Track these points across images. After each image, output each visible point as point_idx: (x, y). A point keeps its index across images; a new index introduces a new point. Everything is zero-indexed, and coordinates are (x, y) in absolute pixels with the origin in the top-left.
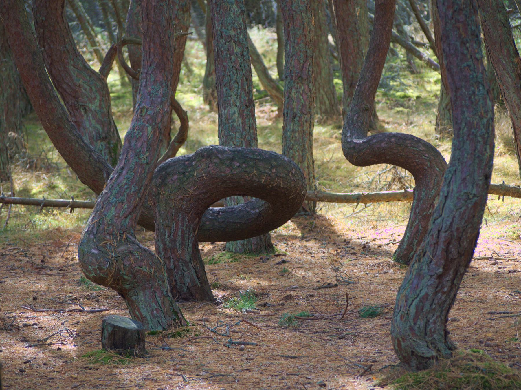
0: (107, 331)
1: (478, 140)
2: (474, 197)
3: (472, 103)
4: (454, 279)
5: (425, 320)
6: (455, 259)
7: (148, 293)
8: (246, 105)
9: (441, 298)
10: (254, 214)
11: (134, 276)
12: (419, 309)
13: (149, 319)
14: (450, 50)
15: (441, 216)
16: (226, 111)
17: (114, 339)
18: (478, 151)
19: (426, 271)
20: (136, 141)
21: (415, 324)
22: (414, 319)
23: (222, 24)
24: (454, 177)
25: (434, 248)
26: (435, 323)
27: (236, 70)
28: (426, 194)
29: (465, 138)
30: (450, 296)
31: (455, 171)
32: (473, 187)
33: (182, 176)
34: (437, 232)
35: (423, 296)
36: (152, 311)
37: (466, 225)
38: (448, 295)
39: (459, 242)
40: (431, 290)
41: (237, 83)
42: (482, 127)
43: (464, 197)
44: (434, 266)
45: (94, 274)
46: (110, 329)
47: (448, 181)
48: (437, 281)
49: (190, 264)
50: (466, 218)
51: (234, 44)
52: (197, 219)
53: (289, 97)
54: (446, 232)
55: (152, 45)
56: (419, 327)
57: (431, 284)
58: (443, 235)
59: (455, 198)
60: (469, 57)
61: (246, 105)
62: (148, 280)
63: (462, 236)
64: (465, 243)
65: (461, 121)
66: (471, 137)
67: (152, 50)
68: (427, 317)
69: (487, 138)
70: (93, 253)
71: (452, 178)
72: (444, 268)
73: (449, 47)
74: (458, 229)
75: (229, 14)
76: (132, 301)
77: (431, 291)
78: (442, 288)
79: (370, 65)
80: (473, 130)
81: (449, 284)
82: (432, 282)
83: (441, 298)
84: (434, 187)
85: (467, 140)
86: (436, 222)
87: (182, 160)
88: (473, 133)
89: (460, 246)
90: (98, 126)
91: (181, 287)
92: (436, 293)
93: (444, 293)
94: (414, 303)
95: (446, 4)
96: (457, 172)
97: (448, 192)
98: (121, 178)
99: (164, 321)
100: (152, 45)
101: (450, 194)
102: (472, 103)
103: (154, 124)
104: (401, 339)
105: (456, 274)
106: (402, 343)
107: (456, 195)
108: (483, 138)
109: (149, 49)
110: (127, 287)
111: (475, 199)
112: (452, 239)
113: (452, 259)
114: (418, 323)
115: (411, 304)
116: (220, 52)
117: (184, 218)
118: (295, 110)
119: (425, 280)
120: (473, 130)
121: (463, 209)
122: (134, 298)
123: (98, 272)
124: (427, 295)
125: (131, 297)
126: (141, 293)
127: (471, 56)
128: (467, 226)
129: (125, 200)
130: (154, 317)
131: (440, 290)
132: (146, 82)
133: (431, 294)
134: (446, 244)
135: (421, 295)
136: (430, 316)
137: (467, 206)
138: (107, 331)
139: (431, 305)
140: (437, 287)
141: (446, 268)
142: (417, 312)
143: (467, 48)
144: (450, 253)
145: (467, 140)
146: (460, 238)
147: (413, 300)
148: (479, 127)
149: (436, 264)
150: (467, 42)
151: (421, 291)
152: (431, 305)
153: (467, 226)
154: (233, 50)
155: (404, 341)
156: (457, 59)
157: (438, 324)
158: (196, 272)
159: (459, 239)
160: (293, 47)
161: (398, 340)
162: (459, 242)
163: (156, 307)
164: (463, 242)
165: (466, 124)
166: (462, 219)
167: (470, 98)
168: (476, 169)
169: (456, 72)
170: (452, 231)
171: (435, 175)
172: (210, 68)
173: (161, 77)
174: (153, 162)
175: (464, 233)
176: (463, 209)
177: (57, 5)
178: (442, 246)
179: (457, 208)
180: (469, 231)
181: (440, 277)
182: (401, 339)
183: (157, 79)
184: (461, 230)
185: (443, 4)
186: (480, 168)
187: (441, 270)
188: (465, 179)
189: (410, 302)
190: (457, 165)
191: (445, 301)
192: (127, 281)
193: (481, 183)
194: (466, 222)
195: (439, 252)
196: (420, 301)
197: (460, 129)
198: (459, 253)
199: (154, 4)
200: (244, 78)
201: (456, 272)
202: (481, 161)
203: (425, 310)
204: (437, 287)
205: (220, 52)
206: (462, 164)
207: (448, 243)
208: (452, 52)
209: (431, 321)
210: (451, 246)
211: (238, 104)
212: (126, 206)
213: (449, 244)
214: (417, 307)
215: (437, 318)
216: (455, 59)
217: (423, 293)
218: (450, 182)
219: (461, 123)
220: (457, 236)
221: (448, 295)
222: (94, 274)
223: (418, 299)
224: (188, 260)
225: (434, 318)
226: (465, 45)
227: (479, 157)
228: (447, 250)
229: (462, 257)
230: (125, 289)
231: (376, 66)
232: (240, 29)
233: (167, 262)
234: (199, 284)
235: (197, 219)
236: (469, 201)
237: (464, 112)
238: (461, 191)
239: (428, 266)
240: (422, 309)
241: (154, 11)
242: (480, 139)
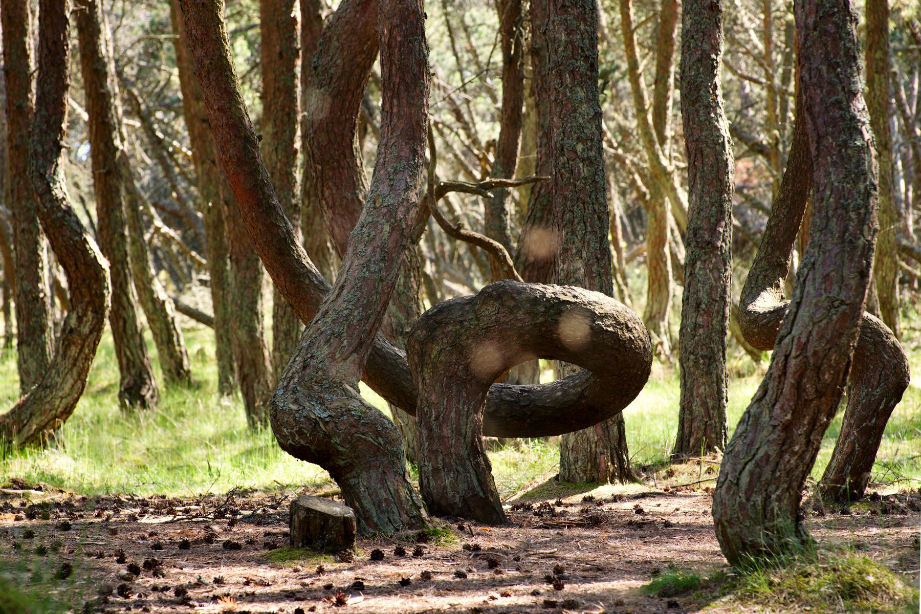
0: (299, 517)
1: (850, 217)
2: (841, 304)
3: (842, 158)
4: (811, 433)
5: (764, 495)
6: (812, 400)
7: (374, 475)
8: (597, 258)
9: (789, 461)
10: (575, 394)
11: (354, 448)
12: (755, 478)
13: (374, 514)
14: (811, 78)
15: (790, 333)
16: (565, 266)
17: (308, 530)
18: (850, 235)
19: (767, 418)
20: (365, 246)
21: (748, 500)
22: (746, 493)
23: (564, 132)
24: (811, 273)
25: (779, 383)
26: (779, 499)
27: (583, 203)
28: (867, 395)
29: (830, 213)
30: (804, 458)
31: (814, 264)
32: (840, 288)
33: (458, 327)
34: (783, 358)
35: (762, 457)
36: (380, 502)
37: (828, 346)
38: (801, 457)
39: (818, 373)
40: (775, 448)
41: (584, 223)
42: (856, 195)
43: (826, 304)
44: (779, 411)
45: (290, 441)
46: (302, 514)
47: (802, 279)
48: (783, 435)
49: (468, 462)
50: (828, 337)
51: (581, 165)
52: (481, 394)
53: (691, 274)
54: (797, 357)
55: (395, 102)
56: (754, 505)
57: (774, 440)
58: (793, 362)
59: (813, 306)
60: (840, 89)
61: (597, 258)
62: (375, 455)
63: (822, 364)
64: (826, 377)
65: (825, 187)
66: (839, 211)
67: (395, 110)
68: (766, 490)
69: (865, 214)
70: (291, 410)
71: (808, 274)
72: (793, 414)
73: (810, 74)
74: (815, 353)
75: (575, 117)
76: (350, 486)
77: (773, 450)
78: (792, 445)
79: (787, 196)
80: (842, 201)
81: (802, 440)
82: (775, 436)
83: (789, 461)
84: (879, 383)
85: (833, 216)
86: (783, 342)
87: (459, 304)
88: (842, 204)
89: (819, 379)
90: (400, 315)
91: (454, 496)
92: (781, 454)
93: (794, 453)
94: (748, 467)
95: (807, 7)
96: (816, 266)
97: (802, 298)
98: (340, 300)
99: (397, 518)
100: (395, 102)
101: (804, 300)
102: (842, 158)
103: (393, 220)
104: (726, 524)
105: (814, 425)
106: (729, 530)
107: (814, 301)
108: (859, 214)
109: (391, 108)
110: (342, 463)
111: (844, 307)
112: (806, 370)
113: (806, 400)
114: (753, 499)
115: (744, 468)
116: (559, 175)
117: (459, 391)
118: (701, 294)
119: (765, 433)
120: (842, 201)
121: (825, 322)
122: (353, 481)
123: (297, 438)
124: (767, 456)
125: (347, 479)
126: (364, 475)
127: (843, 88)
128: (830, 349)
129: (345, 334)
130: (383, 512)
131: (787, 449)
132: (385, 158)
133: (773, 454)
134: (796, 376)
135: (757, 457)
136: (772, 488)
137: (831, 320)
138: (299, 517)
139: (774, 472)
140: (783, 444)
141: (797, 414)
142: (751, 481)
143: (837, 75)
144: (804, 390)
145: (833, 216)
146: (819, 368)
147: (746, 464)
148: (853, 196)
149: (782, 408)
150: (839, 66)
151: (758, 449)
152: (774, 472)
153: (830, 349)
154: (579, 173)
155: (731, 528)
156: (822, 91)
157: (785, 502)
158: (477, 476)
159: (818, 369)
160: (701, 198)
161: (723, 526)
162: (818, 373)
163: (386, 496)
164: (824, 375)
165: (832, 191)
166: (822, 337)
167: (840, 151)
168: (847, 261)
169: (819, 113)
170: (806, 357)
171: (881, 365)
172: (652, 308)
173: (408, 151)
174: (389, 278)
175: (825, 361)
176: (825, 322)
177: (344, 129)
178: (790, 380)
179: (816, 320)
180: (833, 357)
181: (787, 427)
182: (726, 524)
183: (403, 154)
184: (821, 354)
185: (803, 7)
186: (851, 260)
187: (789, 417)
188: (828, 275)
189: (739, 467)
190: (816, 254)
191: (797, 467)
192: (342, 454)
193: (853, 282)
194: (828, 342)
195: (786, 390)
196: (757, 465)
197: (822, 199)
198: (817, 391)
199: (399, 39)
200: (596, 216)
201: (814, 422)
202: (855, 248)
203: (763, 478)
204: (783, 444)
205: (559, 175)
206: (824, 253)
207: (801, 374)
208: (814, 80)
209: (774, 496)
210: (805, 380)
211: (584, 255)
212: (345, 343)
213: (802, 376)
214: (752, 474)
215: (783, 492)
216: (818, 91)
217: (761, 453)
218: (804, 281)
219: (824, 190)
220: (814, 365)
221: (801, 457)
222: (290, 441)
223: (753, 462)
224: (465, 456)
225: (778, 493)
226: (835, 70)
227: (851, 242)
228: (798, 387)
229: (823, 399)
230: (339, 466)
231: (795, 198)
232: (592, 140)
233: (433, 458)
234: (481, 494)
235: (481, 394)
236: (833, 311)
237: (830, 173)
238: (821, 295)
239: (770, 412)
240: (760, 477)
241: (399, 50)
242: (853, 215)
